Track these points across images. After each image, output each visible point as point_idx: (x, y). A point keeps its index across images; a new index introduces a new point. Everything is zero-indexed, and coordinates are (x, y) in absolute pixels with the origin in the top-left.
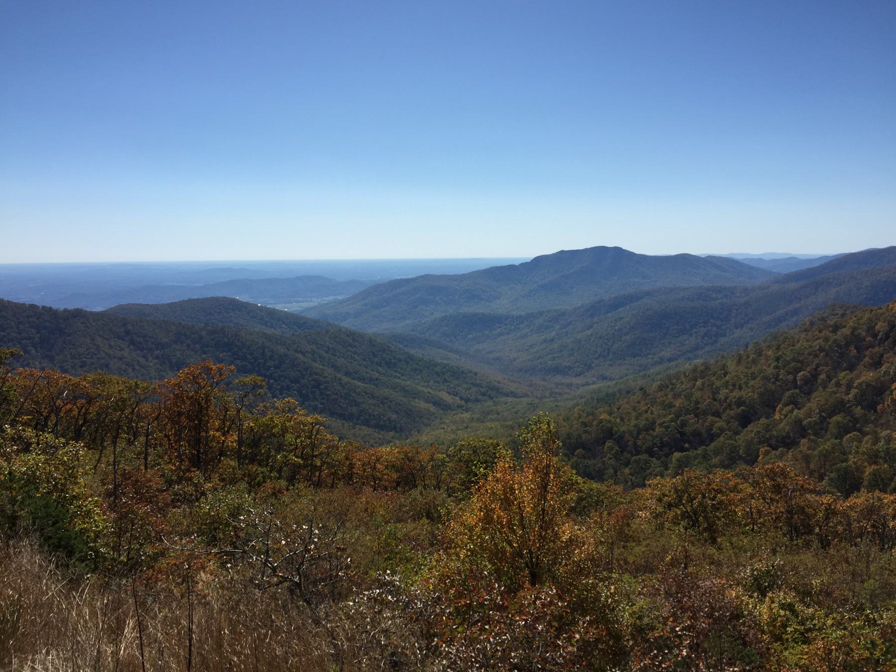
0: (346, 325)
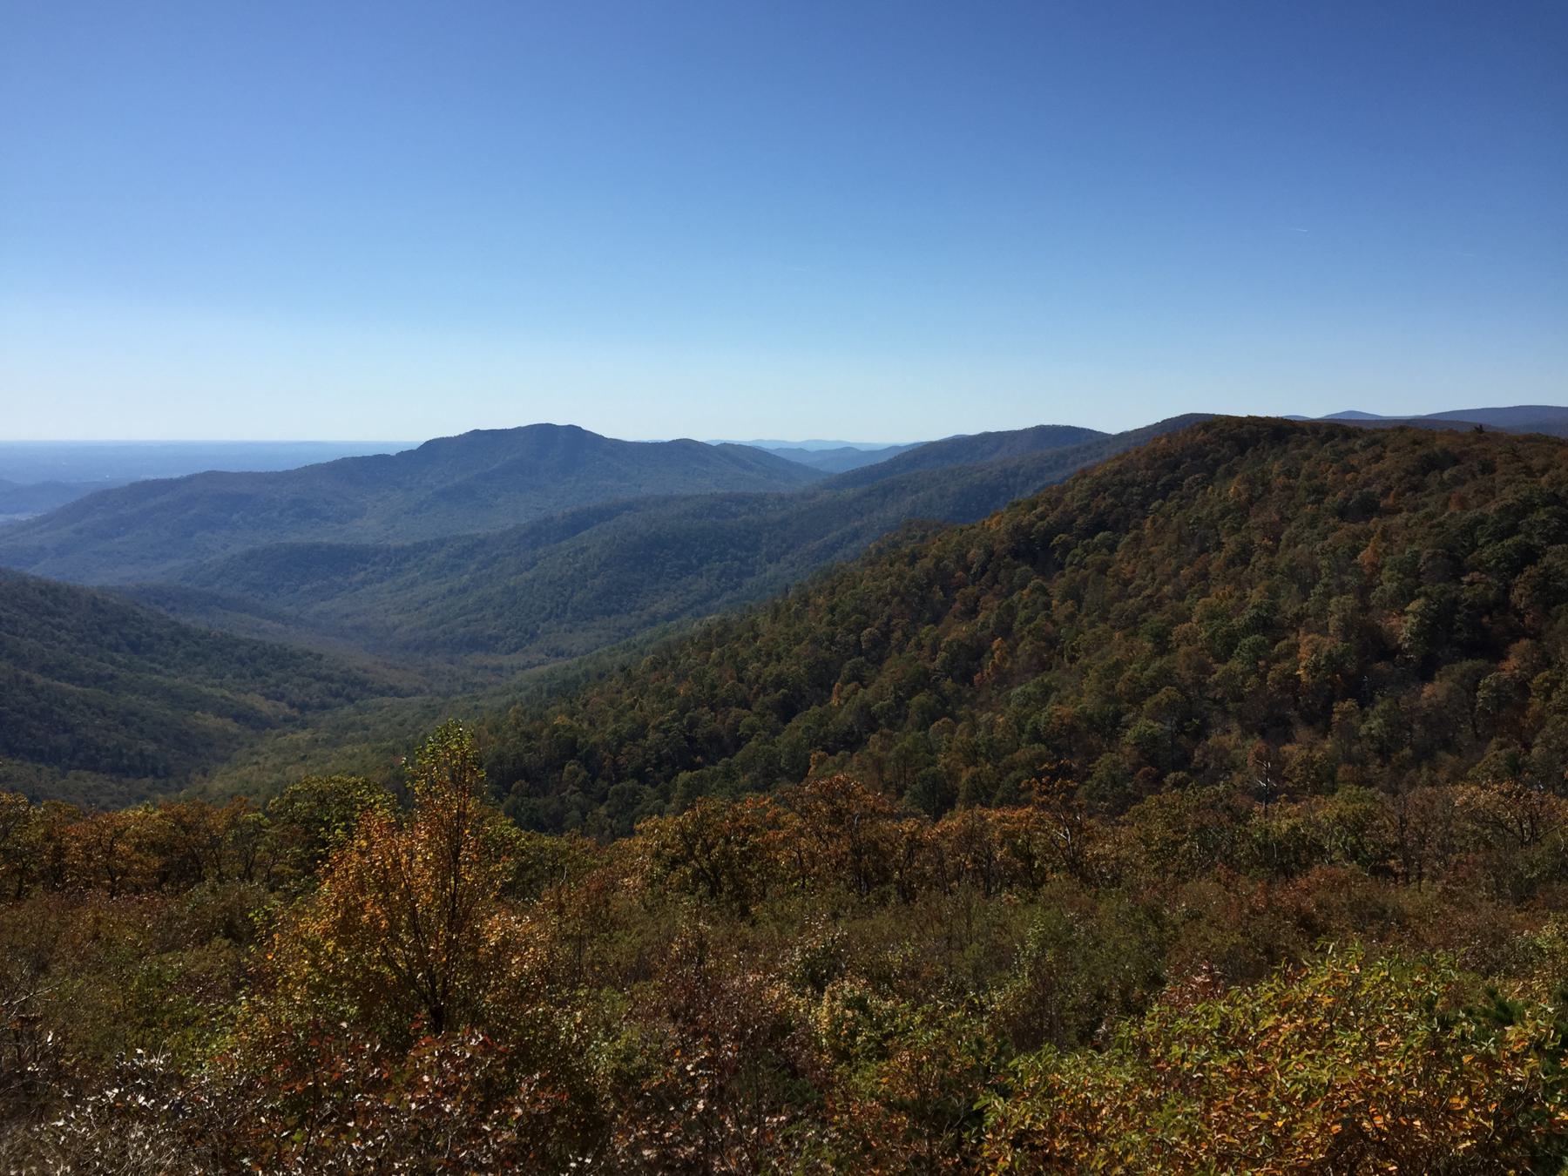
0: (42, 570)
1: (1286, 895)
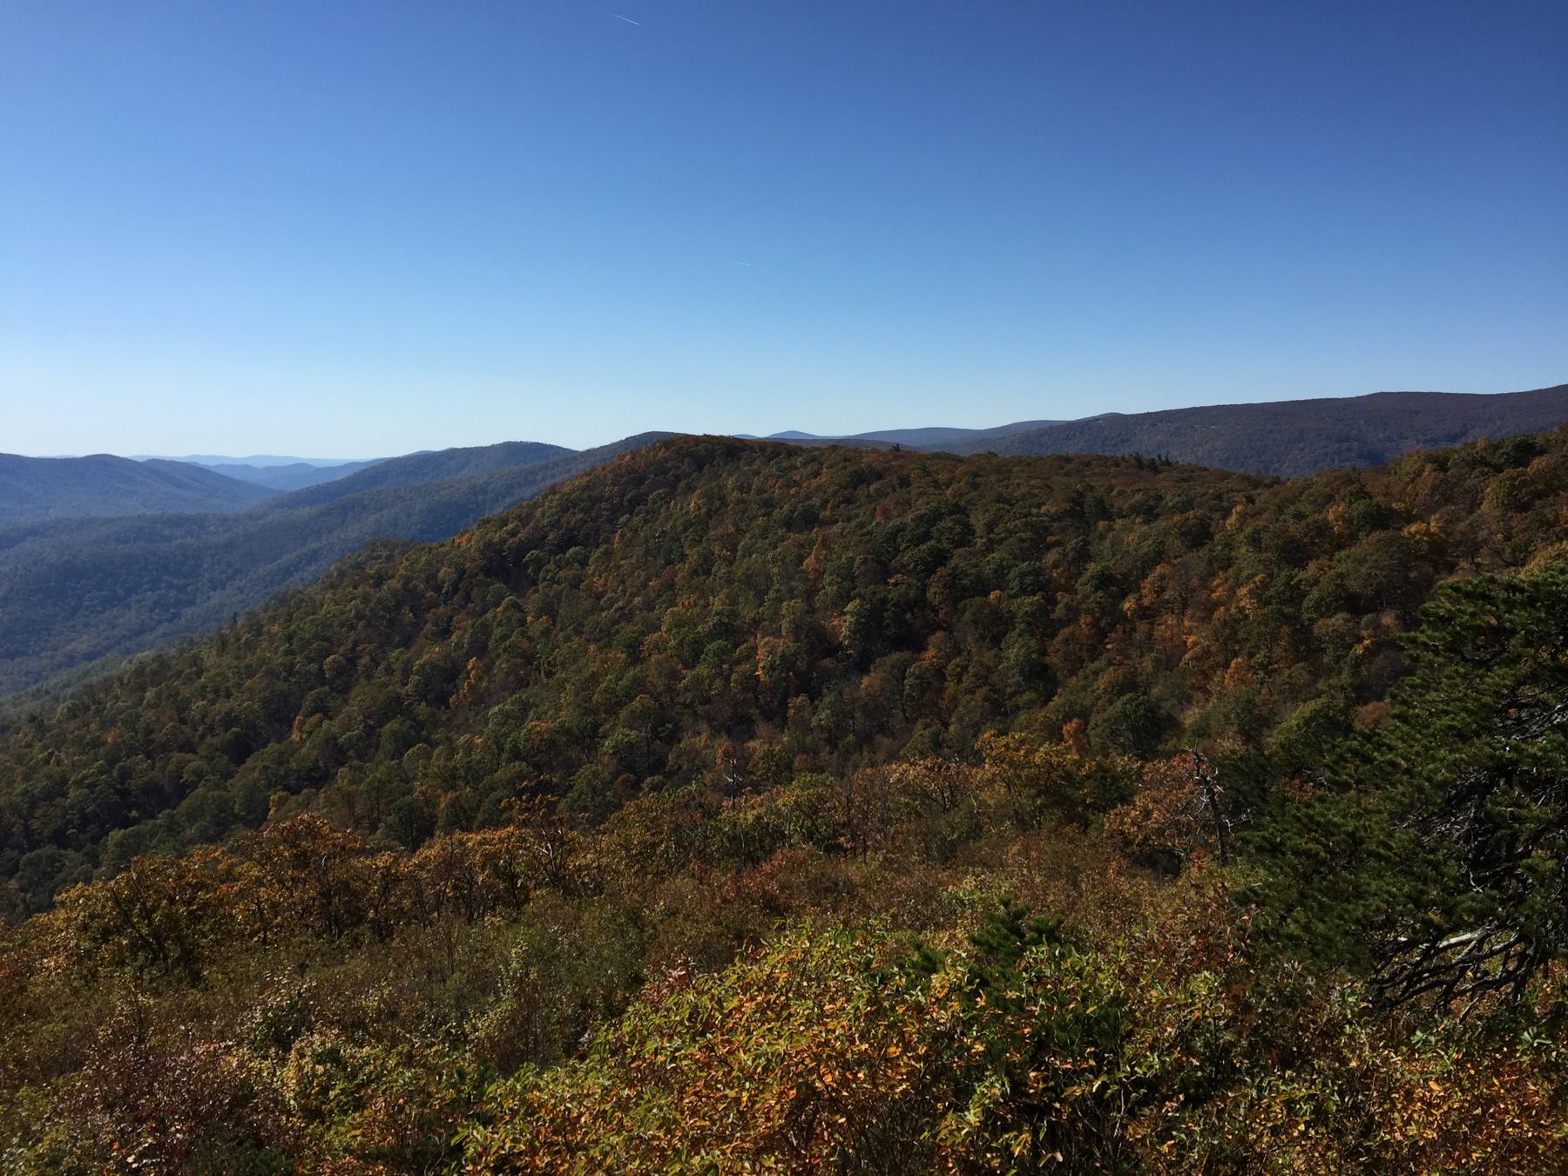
1: (751, 883)
